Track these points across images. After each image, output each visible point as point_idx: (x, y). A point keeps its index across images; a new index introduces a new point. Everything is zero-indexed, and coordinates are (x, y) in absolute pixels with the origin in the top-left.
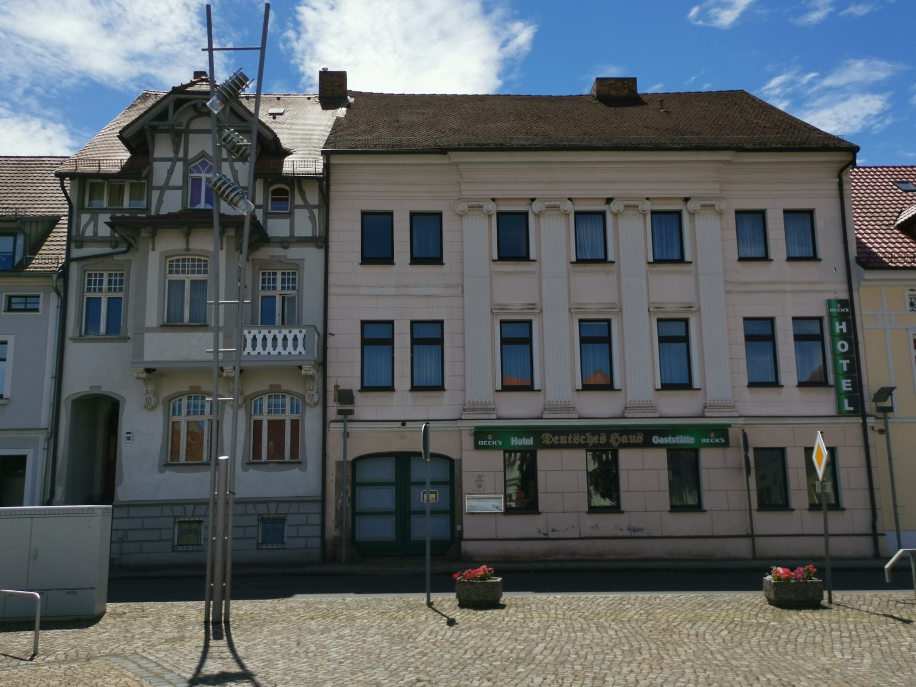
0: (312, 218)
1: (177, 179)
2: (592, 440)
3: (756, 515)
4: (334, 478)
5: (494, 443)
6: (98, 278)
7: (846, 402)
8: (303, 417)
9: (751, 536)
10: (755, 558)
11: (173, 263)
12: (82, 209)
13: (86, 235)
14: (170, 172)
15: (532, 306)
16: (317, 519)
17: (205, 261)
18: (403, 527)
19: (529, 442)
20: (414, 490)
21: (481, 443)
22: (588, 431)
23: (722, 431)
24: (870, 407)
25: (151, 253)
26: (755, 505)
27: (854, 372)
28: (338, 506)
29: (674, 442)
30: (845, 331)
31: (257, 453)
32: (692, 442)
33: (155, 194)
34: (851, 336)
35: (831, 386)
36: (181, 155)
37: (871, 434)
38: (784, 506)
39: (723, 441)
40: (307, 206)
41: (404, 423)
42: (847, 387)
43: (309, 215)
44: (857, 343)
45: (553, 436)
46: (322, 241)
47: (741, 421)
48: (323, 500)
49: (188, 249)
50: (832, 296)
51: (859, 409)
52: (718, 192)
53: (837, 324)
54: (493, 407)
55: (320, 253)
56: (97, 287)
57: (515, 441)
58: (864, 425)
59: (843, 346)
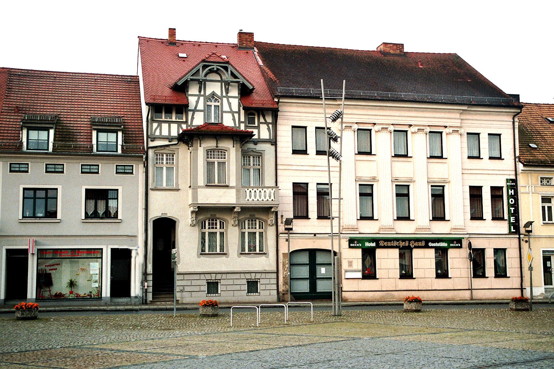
0: (269, 129)
1: (201, 106)
2: (402, 244)
3: (472, 278)
4: (282, 261)
5: (358, 245)
6: (161, 157)
7: (512, 227)
8: (226, 231)
9: (471, 290)
10: (472, 299)
11: (209, 152)
12: (153, 121)
13: (156, 134)
14: (197, 102)
15: (374, 179)
16: (275, 281)
17: (224, 152)
18: (313, 285)
19: (374, 245)
20: (318, 267)
21: (351, 245)
22: (400, 240)
23: (459, 241)
24: (522, 230)
25: (199, 147)
26: (472, 276)
27: (516, 214)
28: (284, 275)
29: (438, 246)
30: (513, 194)
31: (243, 249)
32: (446, 246)
33: (190, 114)
34: (515, 196)
35: (232, 187)
36: (202, 93)
37: (522, 242)
38: (483, 276)
39: (459, 245)
40: (266, 123)
41: (315, 235)
42: (513, 220)
43: (267, 128)
44: (518, 199)
45: (385, 242)
46: (274, 142)
47: (468, 236)
48: (277, 272)
49: (217, 147)
50: (509, 177)
51: (517, 231)
52: (460, 124)
53: (510, 190)
54: (356, 227)
55: (273, 148)
56: (161, 161)
57: (367, 244)
58: (519, 238)
59: (512, 201)
